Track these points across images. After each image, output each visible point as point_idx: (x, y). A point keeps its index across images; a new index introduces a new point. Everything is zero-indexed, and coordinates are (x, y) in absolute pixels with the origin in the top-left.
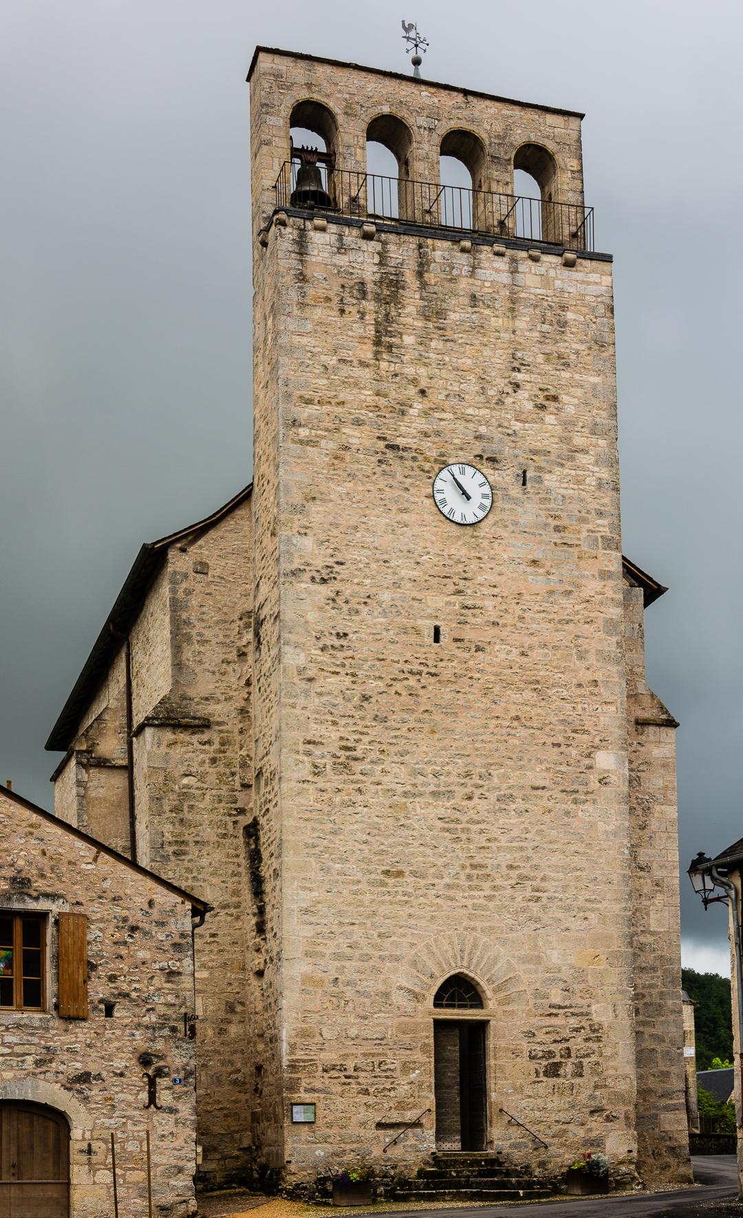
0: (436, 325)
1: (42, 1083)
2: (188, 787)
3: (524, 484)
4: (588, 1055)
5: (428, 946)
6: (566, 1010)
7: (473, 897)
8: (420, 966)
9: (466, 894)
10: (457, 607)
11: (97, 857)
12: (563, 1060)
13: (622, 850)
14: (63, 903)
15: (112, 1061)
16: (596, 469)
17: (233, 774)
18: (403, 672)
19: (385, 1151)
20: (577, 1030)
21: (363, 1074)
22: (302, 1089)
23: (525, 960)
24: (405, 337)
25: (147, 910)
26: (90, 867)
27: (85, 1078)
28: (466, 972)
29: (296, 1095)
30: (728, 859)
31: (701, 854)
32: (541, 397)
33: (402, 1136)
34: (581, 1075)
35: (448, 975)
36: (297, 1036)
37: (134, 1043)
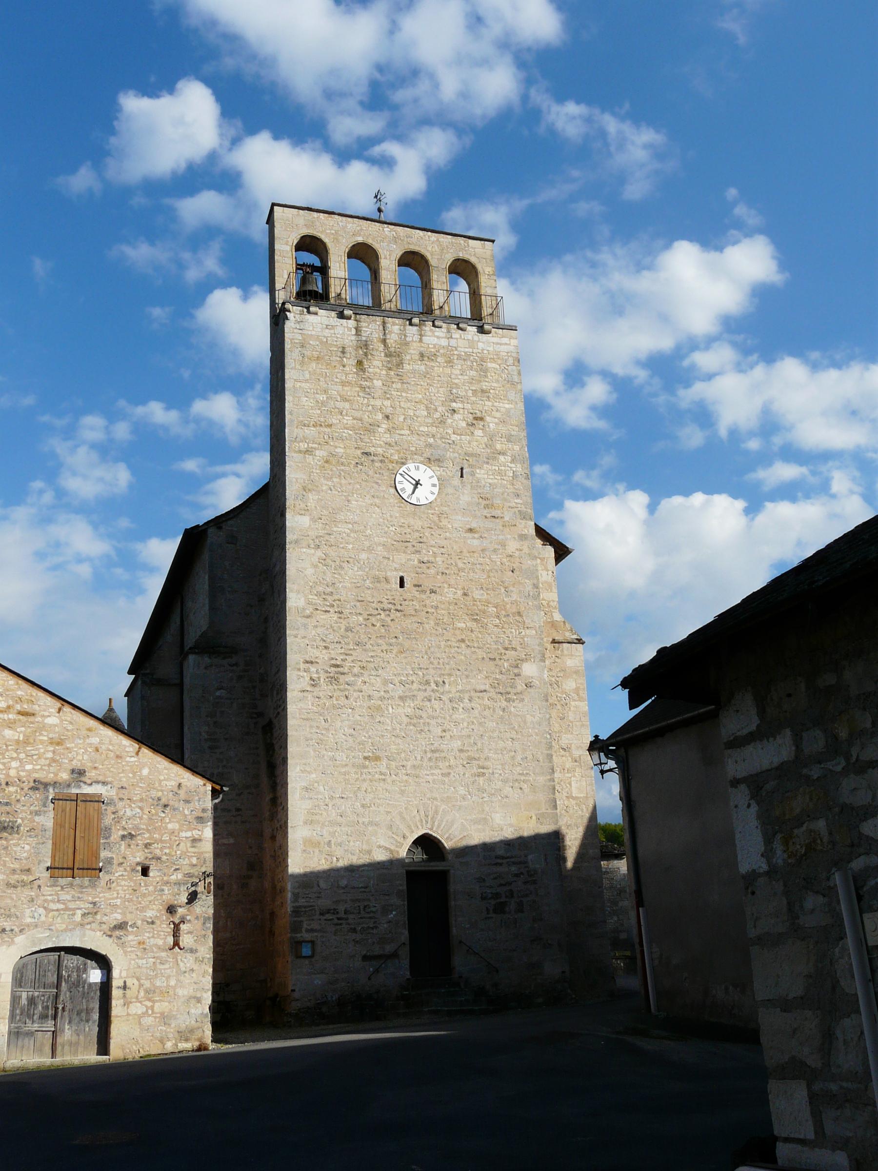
0: (396, 373)
1: (88, 932)
2: (220, 697)
3: (462, 476)
4: (527, 895)
5: (400, 814)
6: (508, 860)
7: (432, 774)
8: (394, 829)
9: (428, 773)
10: (416, 562)
11: (139, 751)
12: (507, 900)
13: (545, 735)
14: (111, 788)
15: (145, 912)
16: (513, 465)
17: (254, 687)
18: (377, 609)
19: (369, 979)
20: (517, 875)
21: (351, 916)
22: (303, 930)
23: (476, 822)
24: (375, 381)
25: (177, 791)
26: (133, 759)
27: (121, 926)
28: (431, 833)
29: (299, 935)
30: (619, 739)
31: (596, 737)
32: (471, 418)
33: (383, 966)
34: (522, 912)
35: (441, 839)
36: (299, 887)
37: (164, 897)
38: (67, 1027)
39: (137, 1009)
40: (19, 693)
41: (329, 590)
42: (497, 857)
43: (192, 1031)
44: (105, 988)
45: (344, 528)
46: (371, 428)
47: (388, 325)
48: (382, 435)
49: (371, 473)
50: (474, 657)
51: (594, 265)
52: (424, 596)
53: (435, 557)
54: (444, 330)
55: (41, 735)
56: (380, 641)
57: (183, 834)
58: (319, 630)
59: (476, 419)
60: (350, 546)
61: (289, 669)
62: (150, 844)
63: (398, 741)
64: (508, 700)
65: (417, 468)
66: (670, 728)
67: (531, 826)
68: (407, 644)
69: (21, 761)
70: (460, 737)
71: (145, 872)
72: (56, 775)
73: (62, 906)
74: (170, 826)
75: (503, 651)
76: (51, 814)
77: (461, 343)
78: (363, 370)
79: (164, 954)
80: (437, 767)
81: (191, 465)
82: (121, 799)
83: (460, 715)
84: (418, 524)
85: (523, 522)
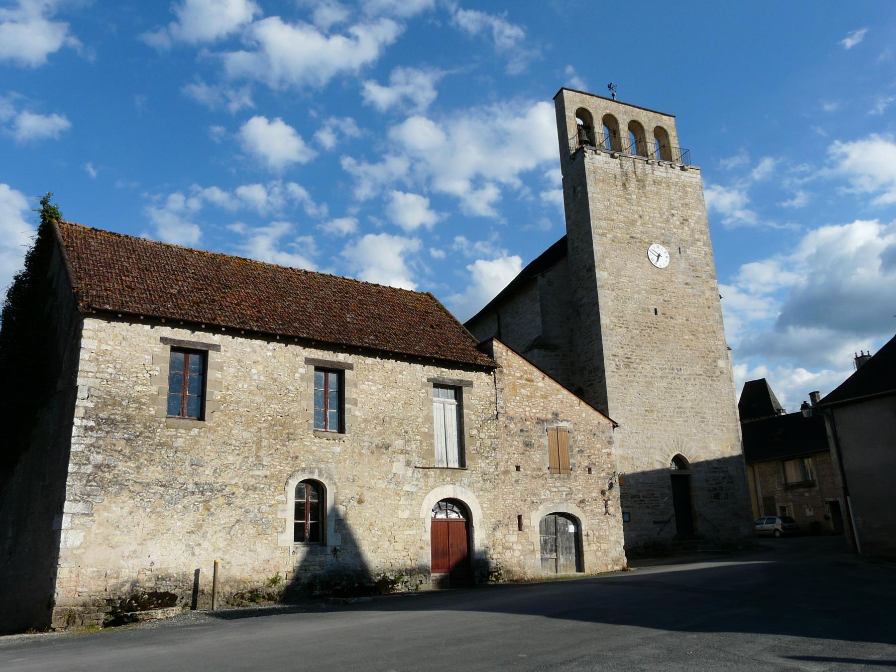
5: (665, 442)
16: (704, 248)
23: (702, 448)
38: (561, 556)
39: (594, 547)
40: (525, 368)
41: (621, 315)
42: (714, 468)
43: (618, 560)
44: (578, 536)
45: (625, 280)
46: (633, 223)
47: (636, 163)
48: (638, 229)
49: (635, 249)
50: (694, 355)
51: (488, 114)
52: (667, 320)
53: (671, 298)
54: (664, 168)
55: (537, 392)
56: (648, 345)
57: (604, 451)
58: (619, 337)
59: (684, 220)
60: (629, 290)
61: (605, 359)
62: (590, 456)
63: (661, 401)
64: (713, 380)
65: (658, 247)
66: (869, 399)
67: (728, 450)
68: (661, 347)
69: (530, 407)
70: (691, 400)
71: (590, 470)
72: (546, 416)
73: (557, 490)
74: (597, 446)
75: (708, 353)
76: (547, 438)
77: (673, 176)
78: (626, 189)
79: (602, 517)
80: (681, 417)
81: (238, 228)
82: (575, 430)
83: (690, 388)
84: (661, 279)
85: (712, 280)
